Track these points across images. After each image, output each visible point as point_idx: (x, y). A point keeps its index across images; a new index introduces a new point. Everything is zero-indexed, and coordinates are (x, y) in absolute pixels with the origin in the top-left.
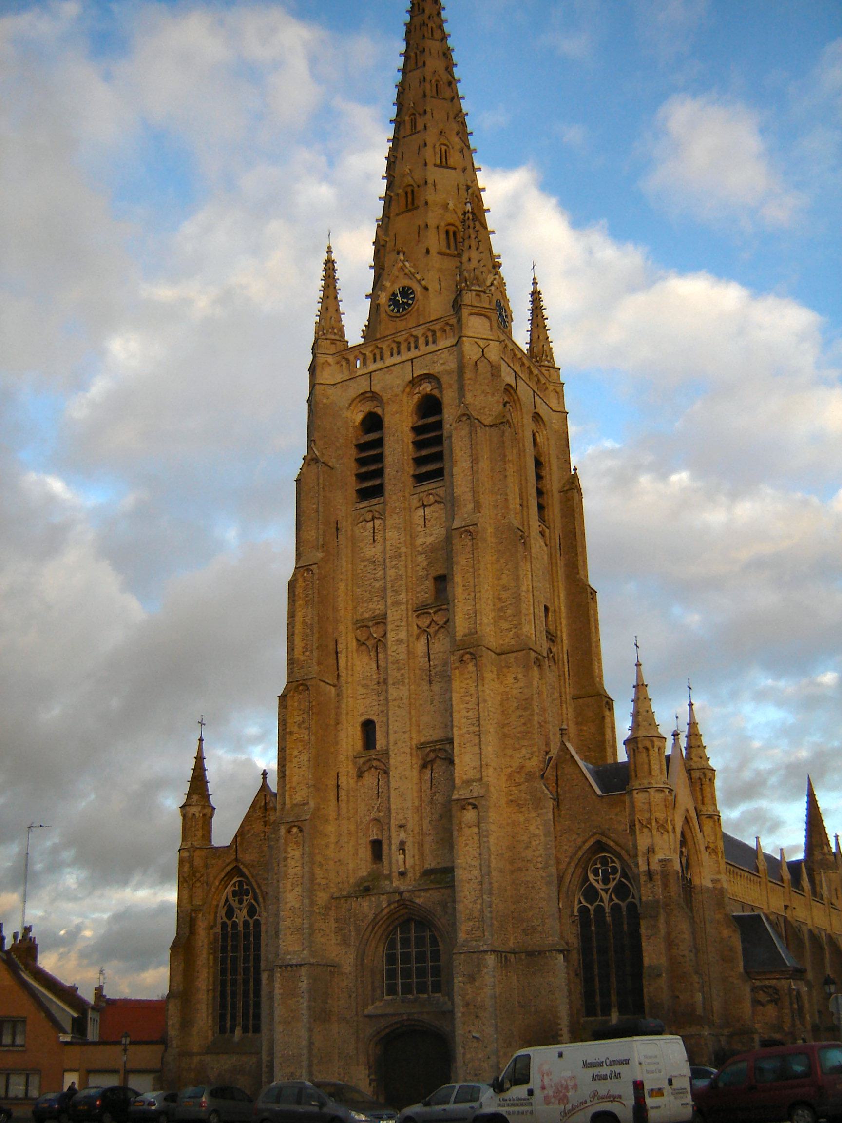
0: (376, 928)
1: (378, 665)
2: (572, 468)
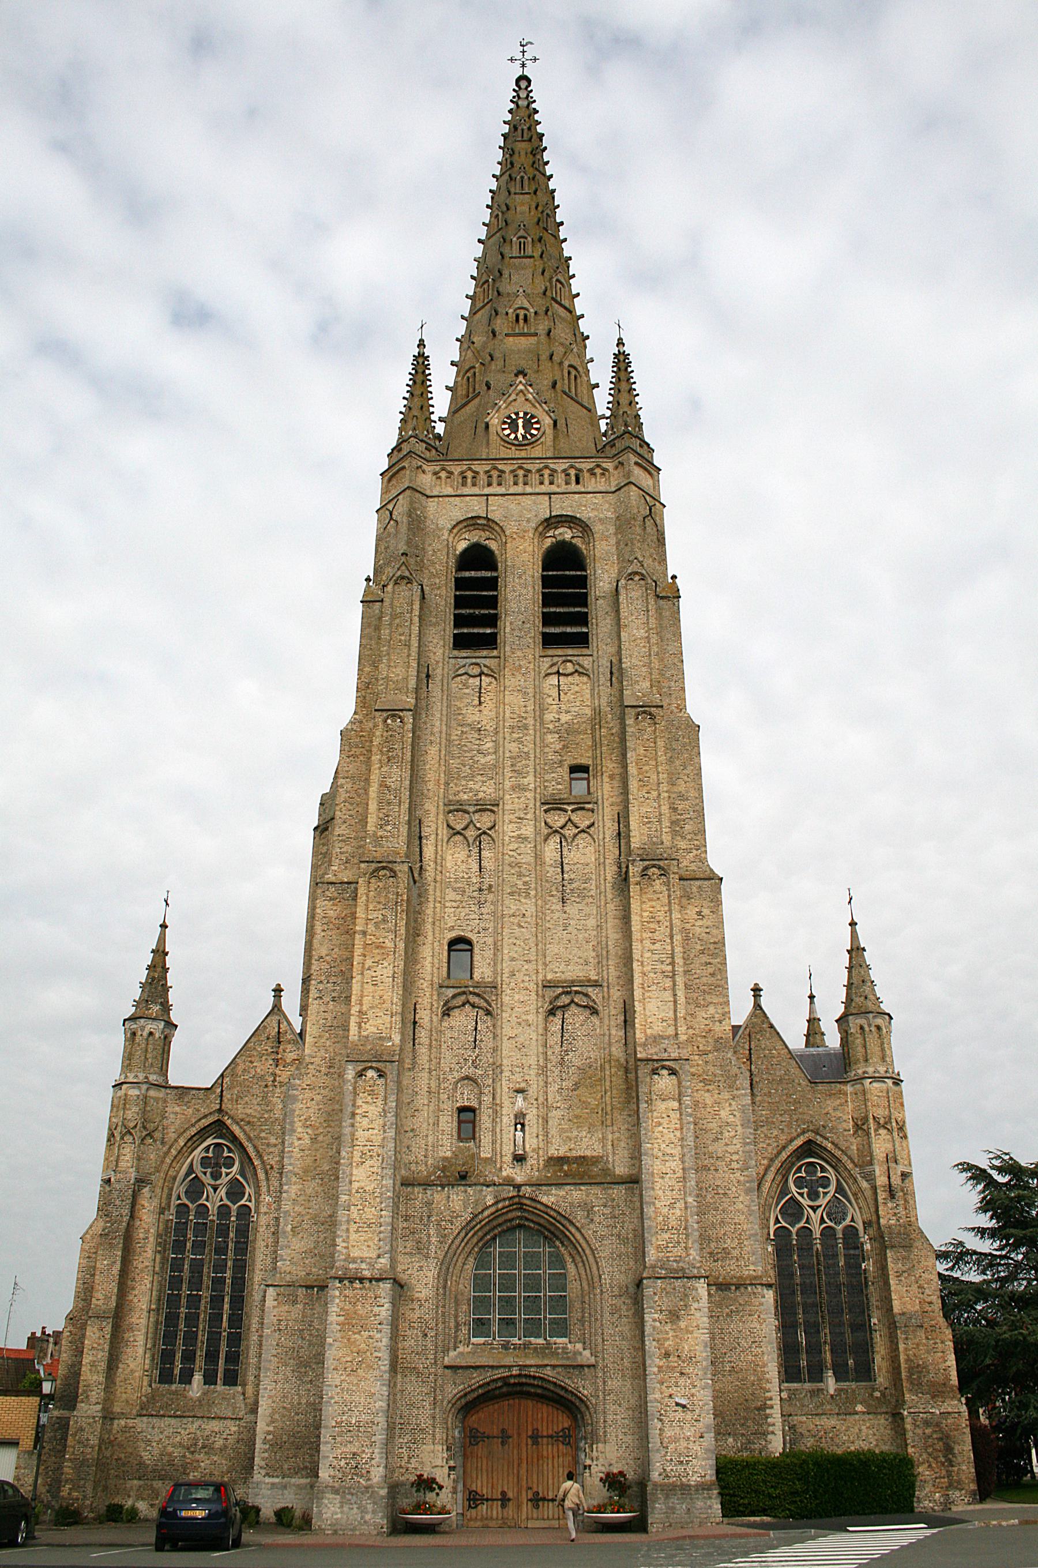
0: (470, 1235)
1: (480, 865)
2: (670, 576)
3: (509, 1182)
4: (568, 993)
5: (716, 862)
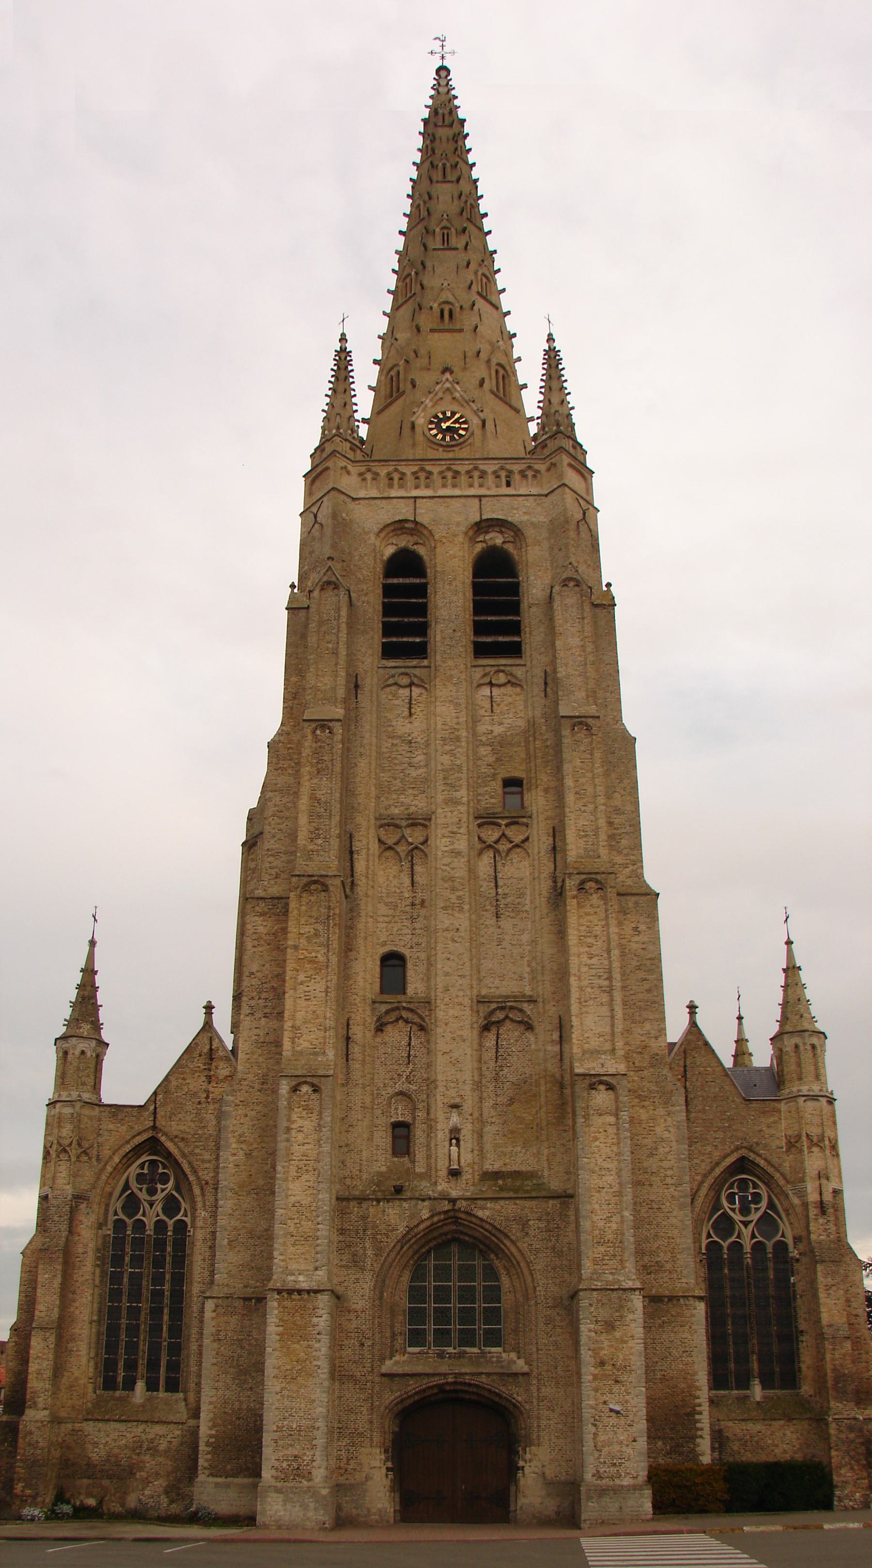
0: (405, 1248)
1: (412, 880)
2: (604, 583)
3: (444, 1197)
4: (502, 1008)
5: (652, 877)
